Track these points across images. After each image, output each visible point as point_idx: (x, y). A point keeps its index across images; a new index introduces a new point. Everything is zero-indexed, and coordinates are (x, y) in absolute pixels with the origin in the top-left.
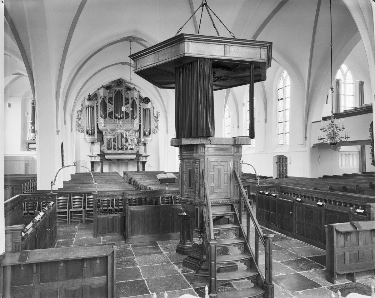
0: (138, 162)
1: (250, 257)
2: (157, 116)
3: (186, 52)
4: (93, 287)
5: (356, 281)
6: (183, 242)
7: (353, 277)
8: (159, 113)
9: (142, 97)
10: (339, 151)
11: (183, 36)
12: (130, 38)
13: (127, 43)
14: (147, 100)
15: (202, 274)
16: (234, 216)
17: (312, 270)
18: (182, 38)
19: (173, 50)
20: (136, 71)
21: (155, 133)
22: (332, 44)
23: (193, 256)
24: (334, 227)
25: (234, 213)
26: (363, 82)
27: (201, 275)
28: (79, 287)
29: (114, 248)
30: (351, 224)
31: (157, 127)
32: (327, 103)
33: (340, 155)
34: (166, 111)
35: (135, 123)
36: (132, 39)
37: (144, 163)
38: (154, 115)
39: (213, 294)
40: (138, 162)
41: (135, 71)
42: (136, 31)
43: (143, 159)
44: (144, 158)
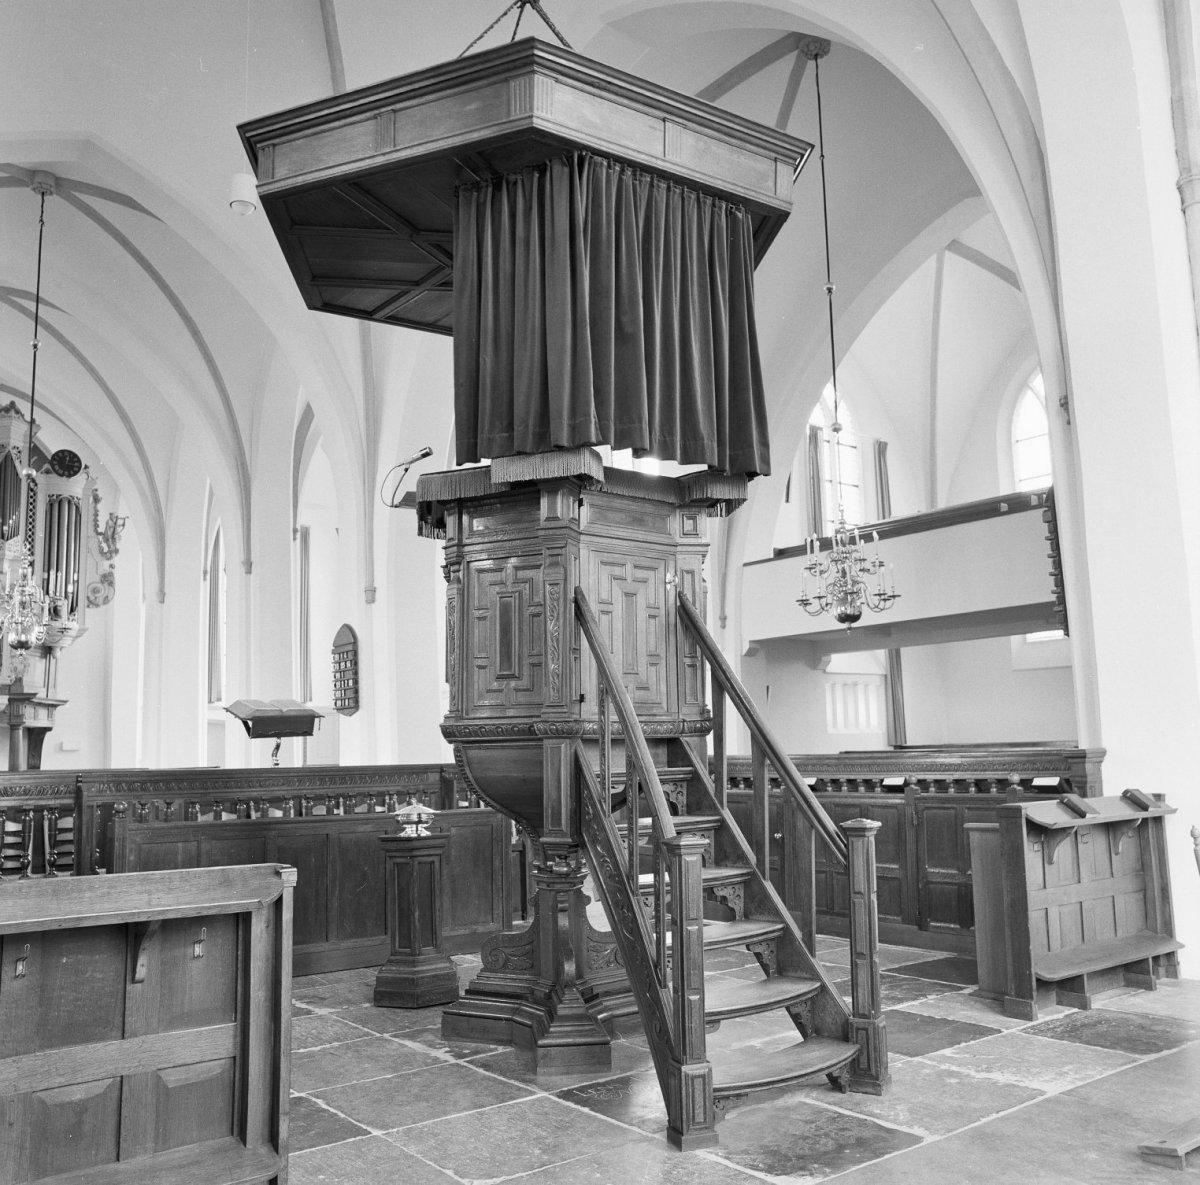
0: (13, 728)
1: (780, 926)
2: (110, 533)
3: (536, 113)
4: (172, 1079)
5: (1093, 1006)
6: (406, 954)
7: (1082, 989)
8: (120, 522)
9: (46, 448)
10: (824, 672)
11: (533, 48)
12: (38, 179)
13: (28, 196)
14: (67, 463)
15: (567, 1034)
16: (685, 784)
17: (930, 997)
18: (528, 56)
19: (473, 106)
20: (265, 188)
21: (97, 606)
22: (832, 284)
23: (492, 989)
24: (1023, 811)
25: (690, 772)
26: (886, 444)
27: (559, 1041)
28: (98, 1088)
29: (284, 876)
30: (1062, 802)
31: (108, 579)
32: (787, 501)
33: (828, 687)
34: (159, 509)
35: (9, 555)
36: (53, 184)
37: (36, 736)
38: (96, 526)
39: (699, 1066)
40: (13, 728)
41: (261, 190)
42: (88, 146)
43: (35, 717)
44: (43, 712)
